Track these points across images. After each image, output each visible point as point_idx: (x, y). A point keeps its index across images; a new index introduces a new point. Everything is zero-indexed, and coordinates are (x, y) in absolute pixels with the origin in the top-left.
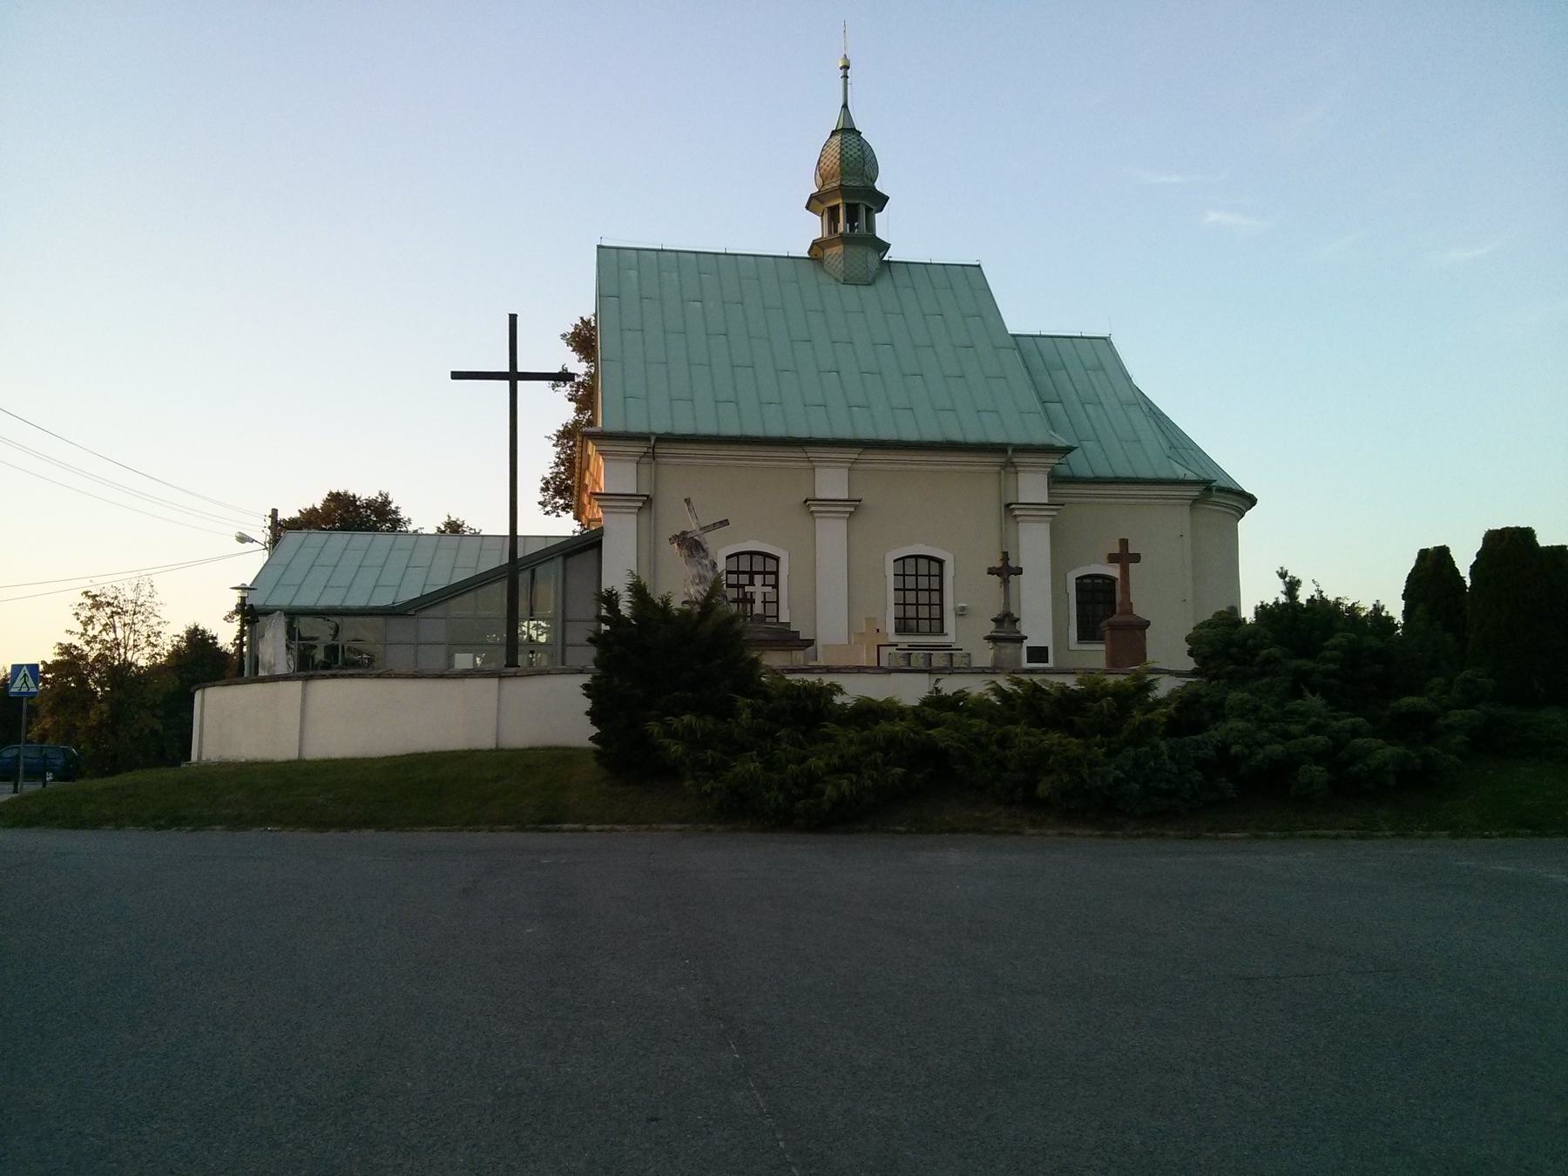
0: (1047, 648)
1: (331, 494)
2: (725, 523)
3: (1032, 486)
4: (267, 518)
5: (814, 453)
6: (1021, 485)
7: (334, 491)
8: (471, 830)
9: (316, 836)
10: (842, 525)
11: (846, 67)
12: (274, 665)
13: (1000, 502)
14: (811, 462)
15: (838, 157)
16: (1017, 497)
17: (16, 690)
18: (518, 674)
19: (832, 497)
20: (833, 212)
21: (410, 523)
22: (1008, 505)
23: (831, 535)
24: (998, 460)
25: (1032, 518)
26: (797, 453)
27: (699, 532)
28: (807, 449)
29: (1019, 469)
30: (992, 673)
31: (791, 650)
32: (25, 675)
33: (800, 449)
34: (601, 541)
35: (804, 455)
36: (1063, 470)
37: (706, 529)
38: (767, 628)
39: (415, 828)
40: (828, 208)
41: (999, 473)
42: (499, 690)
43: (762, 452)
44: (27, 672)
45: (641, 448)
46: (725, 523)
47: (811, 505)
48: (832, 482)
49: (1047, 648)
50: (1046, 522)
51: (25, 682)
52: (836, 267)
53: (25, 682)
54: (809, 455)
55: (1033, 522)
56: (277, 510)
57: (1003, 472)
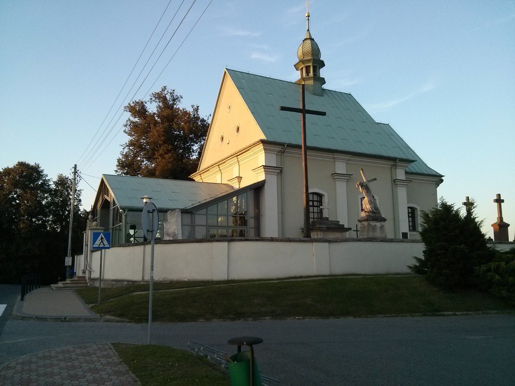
0: (407, 233)
1: (19, 163)
2: (375, 179)
3: (400, 174)
4: (72, 169)
5: (336, 156)
6: (397, 173)
7: (20, 161)
8: (402, 316)
9: (321, 320)
10: (344, 184)
11: (309, 16)
12: (178, 234)
13: (392, 179)
14: (334, 159)
15: (311, 48)
16: (396, 178)
17: (97, 246)
18: (337, 241)
19: (339, 173)
20: (308, 68)
21: (47, 176)
22: (394, 180)
23: (341, 187)
24: (390, 163)
25: (401, 185)
26: (330, 155)
27: (367, 183)
28: (335, 154)
29: (397, 167)
30: (412, 242)
31: (342, 232)
32: (102, 238)
33: (332, 154)
34: (265, 184)
35: (333, 156)
36: (408, 170)
37: (369, 181)
38: (332, 223)
39: (369, 316)
40: (306, 66)
41: (391, 168)
42: (228, 246)
43: (319, 154)
44: (103, 236)
45: (278, 148)
46: (375, 179)
47: (335, 175)
48: (341, 167)
49: (407, 233)
50: (405, 187)
51: (102, 241)
52: (310, 88)
53: (102, 241)
54: (335, 156)
55: (402, 187)
56: (76, 165)
57: (392, 168)
